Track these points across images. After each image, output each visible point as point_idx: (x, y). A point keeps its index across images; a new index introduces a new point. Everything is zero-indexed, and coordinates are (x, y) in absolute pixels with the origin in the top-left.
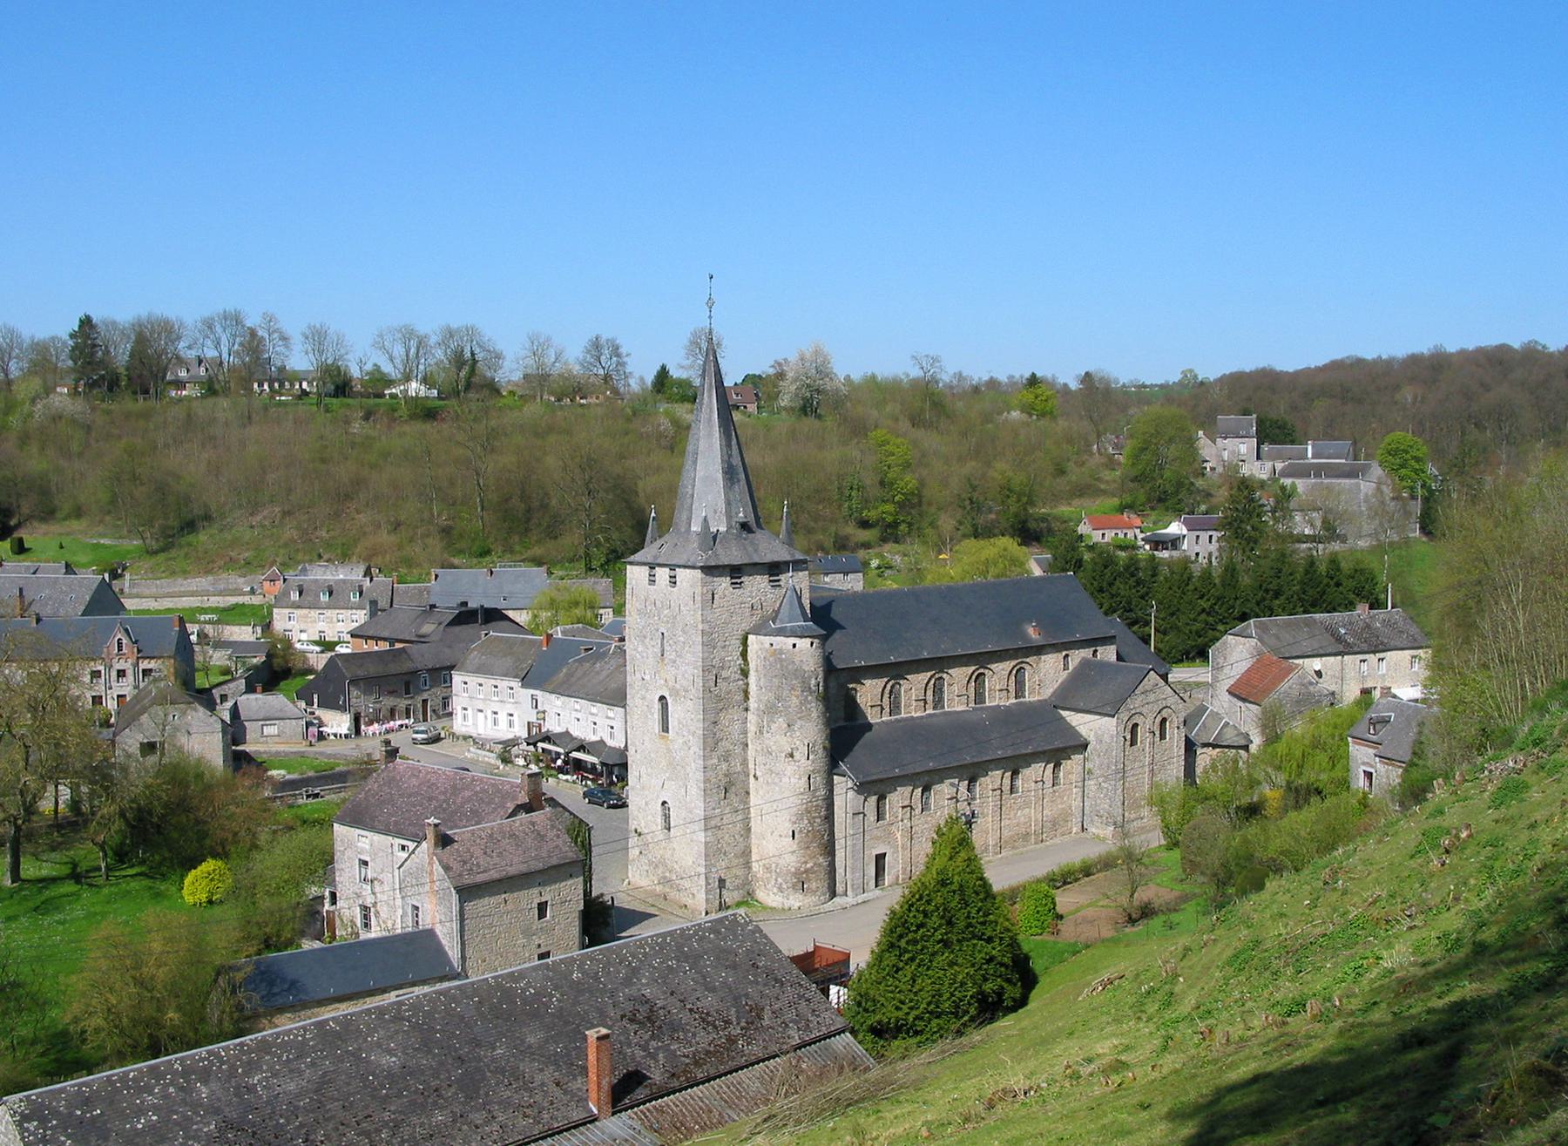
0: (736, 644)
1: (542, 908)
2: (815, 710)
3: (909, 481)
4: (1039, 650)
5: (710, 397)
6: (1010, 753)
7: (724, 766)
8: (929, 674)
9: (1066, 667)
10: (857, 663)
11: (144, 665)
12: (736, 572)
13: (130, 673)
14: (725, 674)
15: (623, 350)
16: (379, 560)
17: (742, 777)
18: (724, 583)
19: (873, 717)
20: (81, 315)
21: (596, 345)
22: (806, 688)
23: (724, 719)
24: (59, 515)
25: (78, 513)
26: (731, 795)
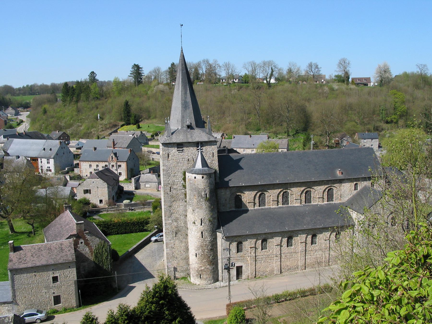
0: (181, 175)
1: (55, 279)
2: (205, 205)
3: (404, 107)
4: (341, 181)
5: (179, 74)
6: (310, 227)
7: (175, 224)
8: (304, 188)
9: (356, 189)
10: (240, 184)
11: (119, 164)
12: (180, 146)
13: (115, 166)
14: (175, 187)
15: (319, 67)
16: (227, 132)
17: (184, 228)
18: (174, 151)
19: (250, 207)
20: (172, 63)
21: (310, 65)
22: (200, 195)
23: (175, 205)
24: (151, 118)
25: (155, 117)
26: (179, 235)
